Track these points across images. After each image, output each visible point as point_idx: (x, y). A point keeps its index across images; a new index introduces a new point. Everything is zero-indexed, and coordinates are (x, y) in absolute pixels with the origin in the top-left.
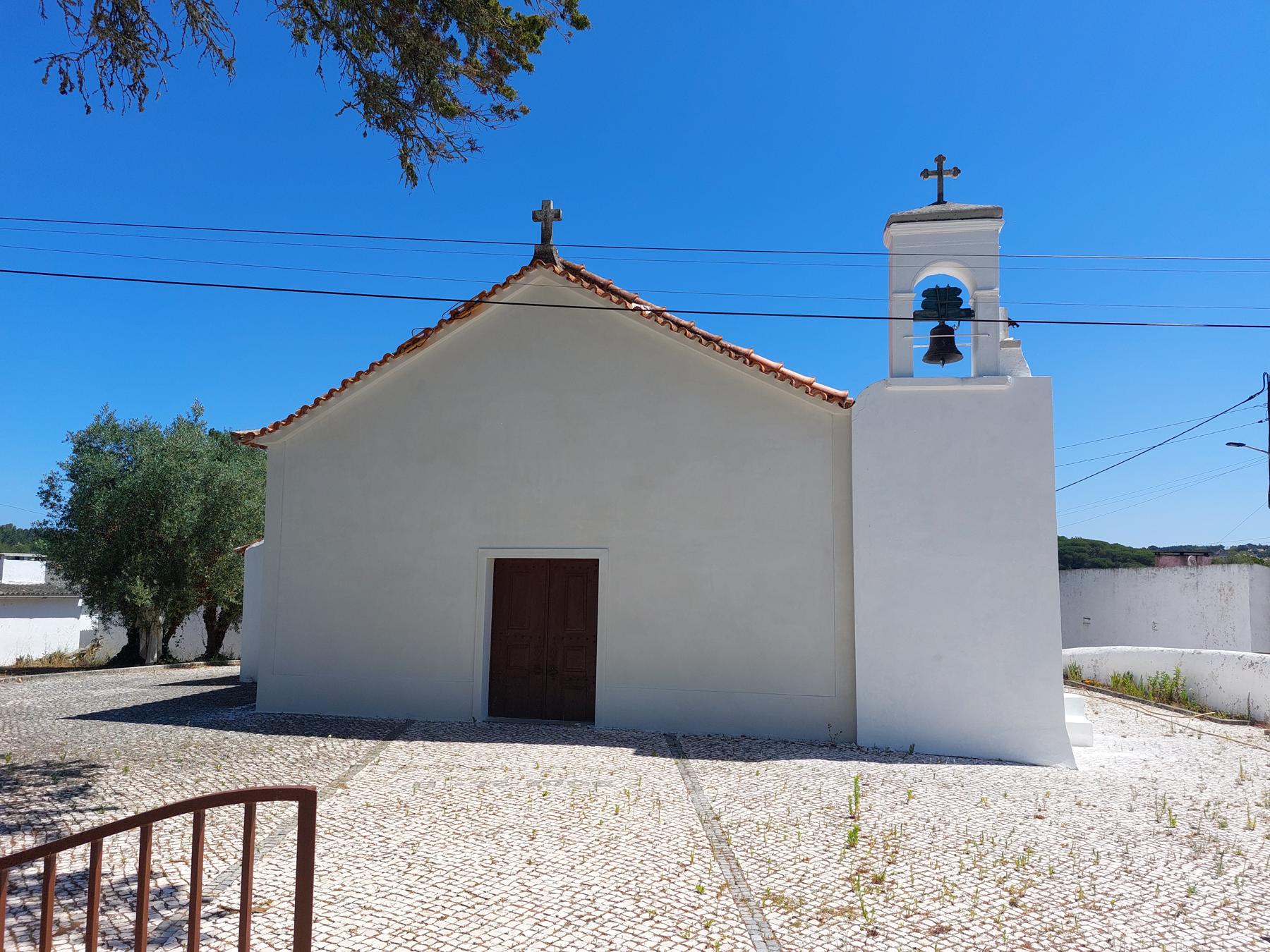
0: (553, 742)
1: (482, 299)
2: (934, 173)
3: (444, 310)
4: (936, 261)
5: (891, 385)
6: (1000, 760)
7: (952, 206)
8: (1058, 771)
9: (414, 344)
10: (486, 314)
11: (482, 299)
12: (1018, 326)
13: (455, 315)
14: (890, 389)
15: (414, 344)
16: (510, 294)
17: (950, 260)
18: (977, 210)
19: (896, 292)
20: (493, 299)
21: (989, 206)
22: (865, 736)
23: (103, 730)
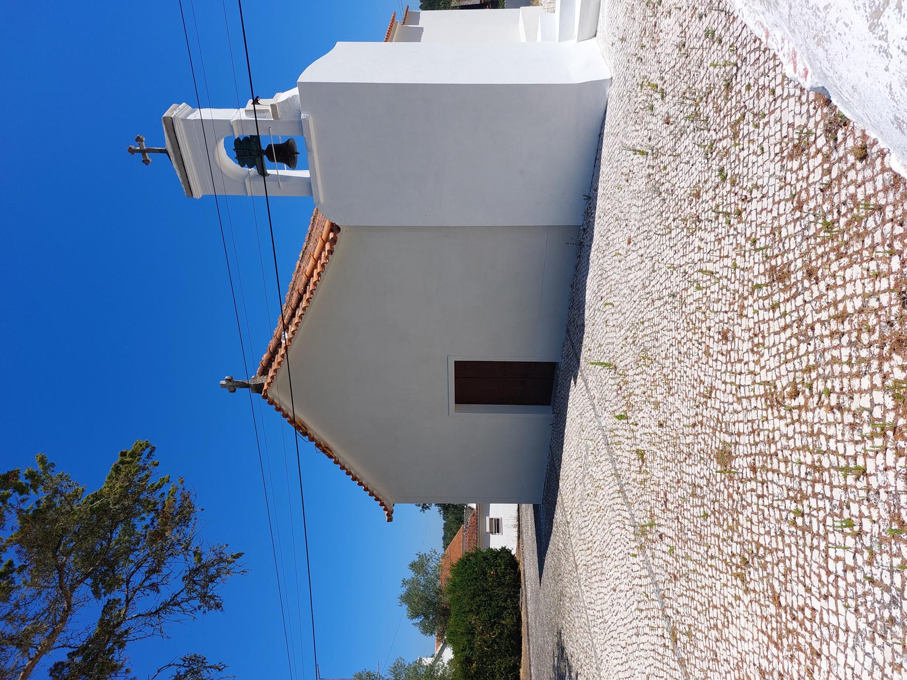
0: (565, 422)
1: (292, 421)
2: (144, 156)
3: (303, 441)
4: (215, 161)
5: (319, 201)
6: (600, 136)
7: (168, 146)
8: (612, 92)
9: (325, 450)
10: (301, 416)
11: (292, 421)
12: (258, 97)
13: (305, 434)
14: (322, 200)
15: (325, 450)
16: (286, 405)
17: (214, 155)
18: (169, 136)
19: (246, 192)
20: (291, 414)
21: (164, 126)
22: (578, 221)
23: (619, 238)
